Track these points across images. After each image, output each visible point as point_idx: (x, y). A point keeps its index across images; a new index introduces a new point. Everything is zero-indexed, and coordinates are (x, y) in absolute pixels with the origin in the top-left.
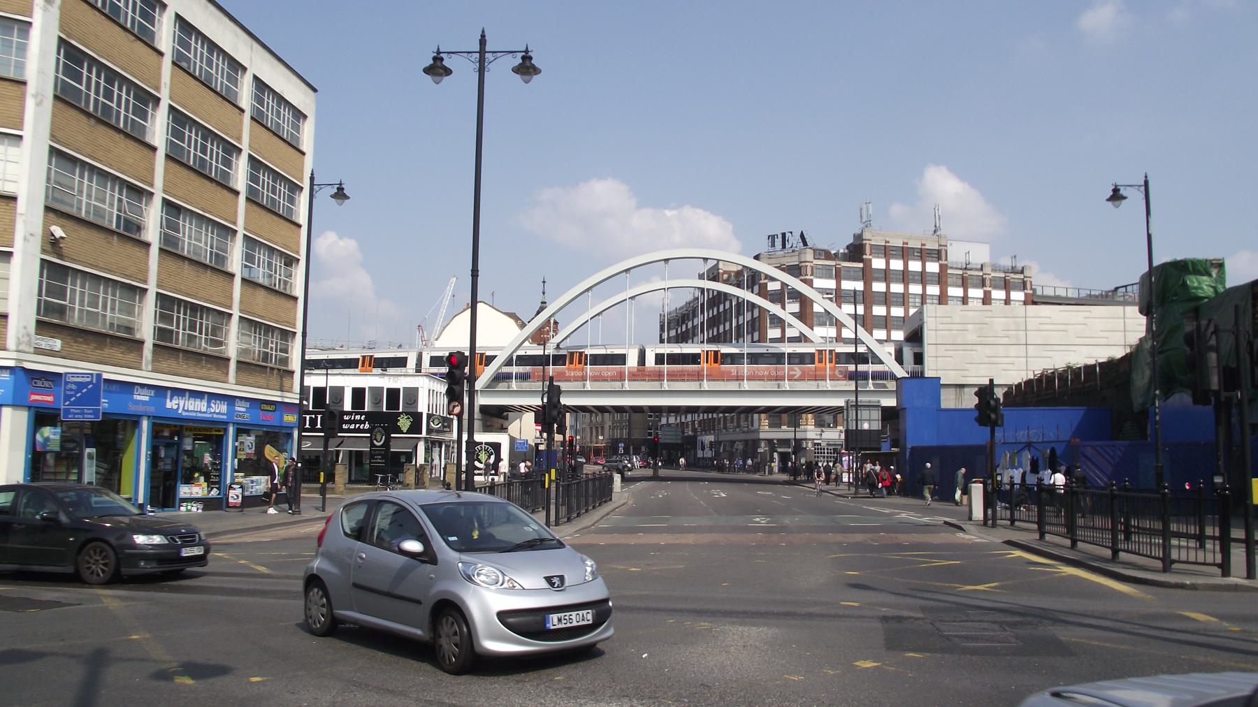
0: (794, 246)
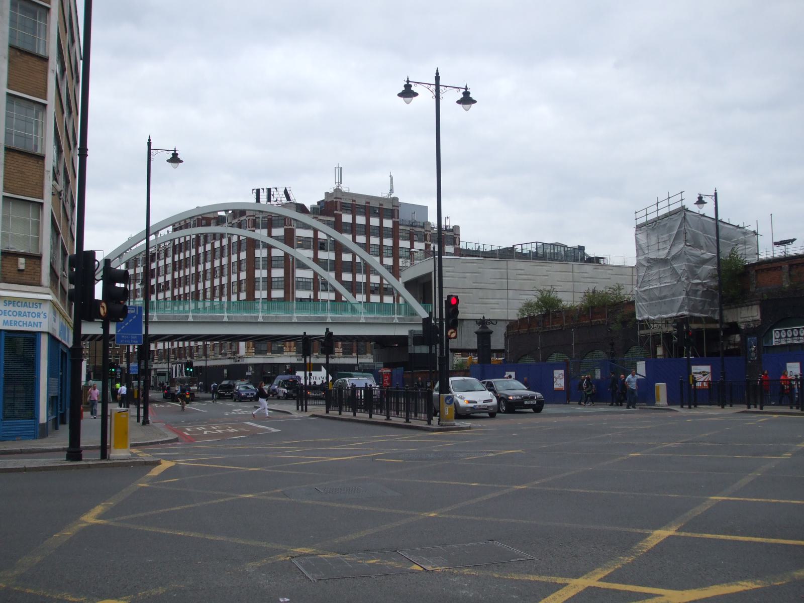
0: (279, 199)
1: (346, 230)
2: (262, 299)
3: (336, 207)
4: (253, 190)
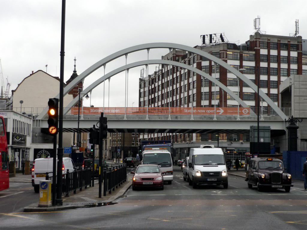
0: (217, 41)
1: (263, 59)
2: (263, 107)
3: (256, 44)
4: (201, 36)
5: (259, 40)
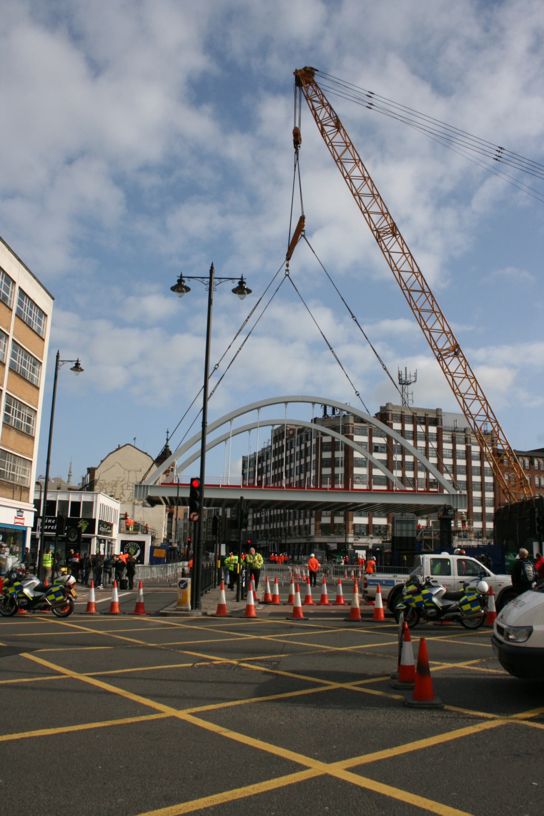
3: (388, 417)
5: (393, 412)
